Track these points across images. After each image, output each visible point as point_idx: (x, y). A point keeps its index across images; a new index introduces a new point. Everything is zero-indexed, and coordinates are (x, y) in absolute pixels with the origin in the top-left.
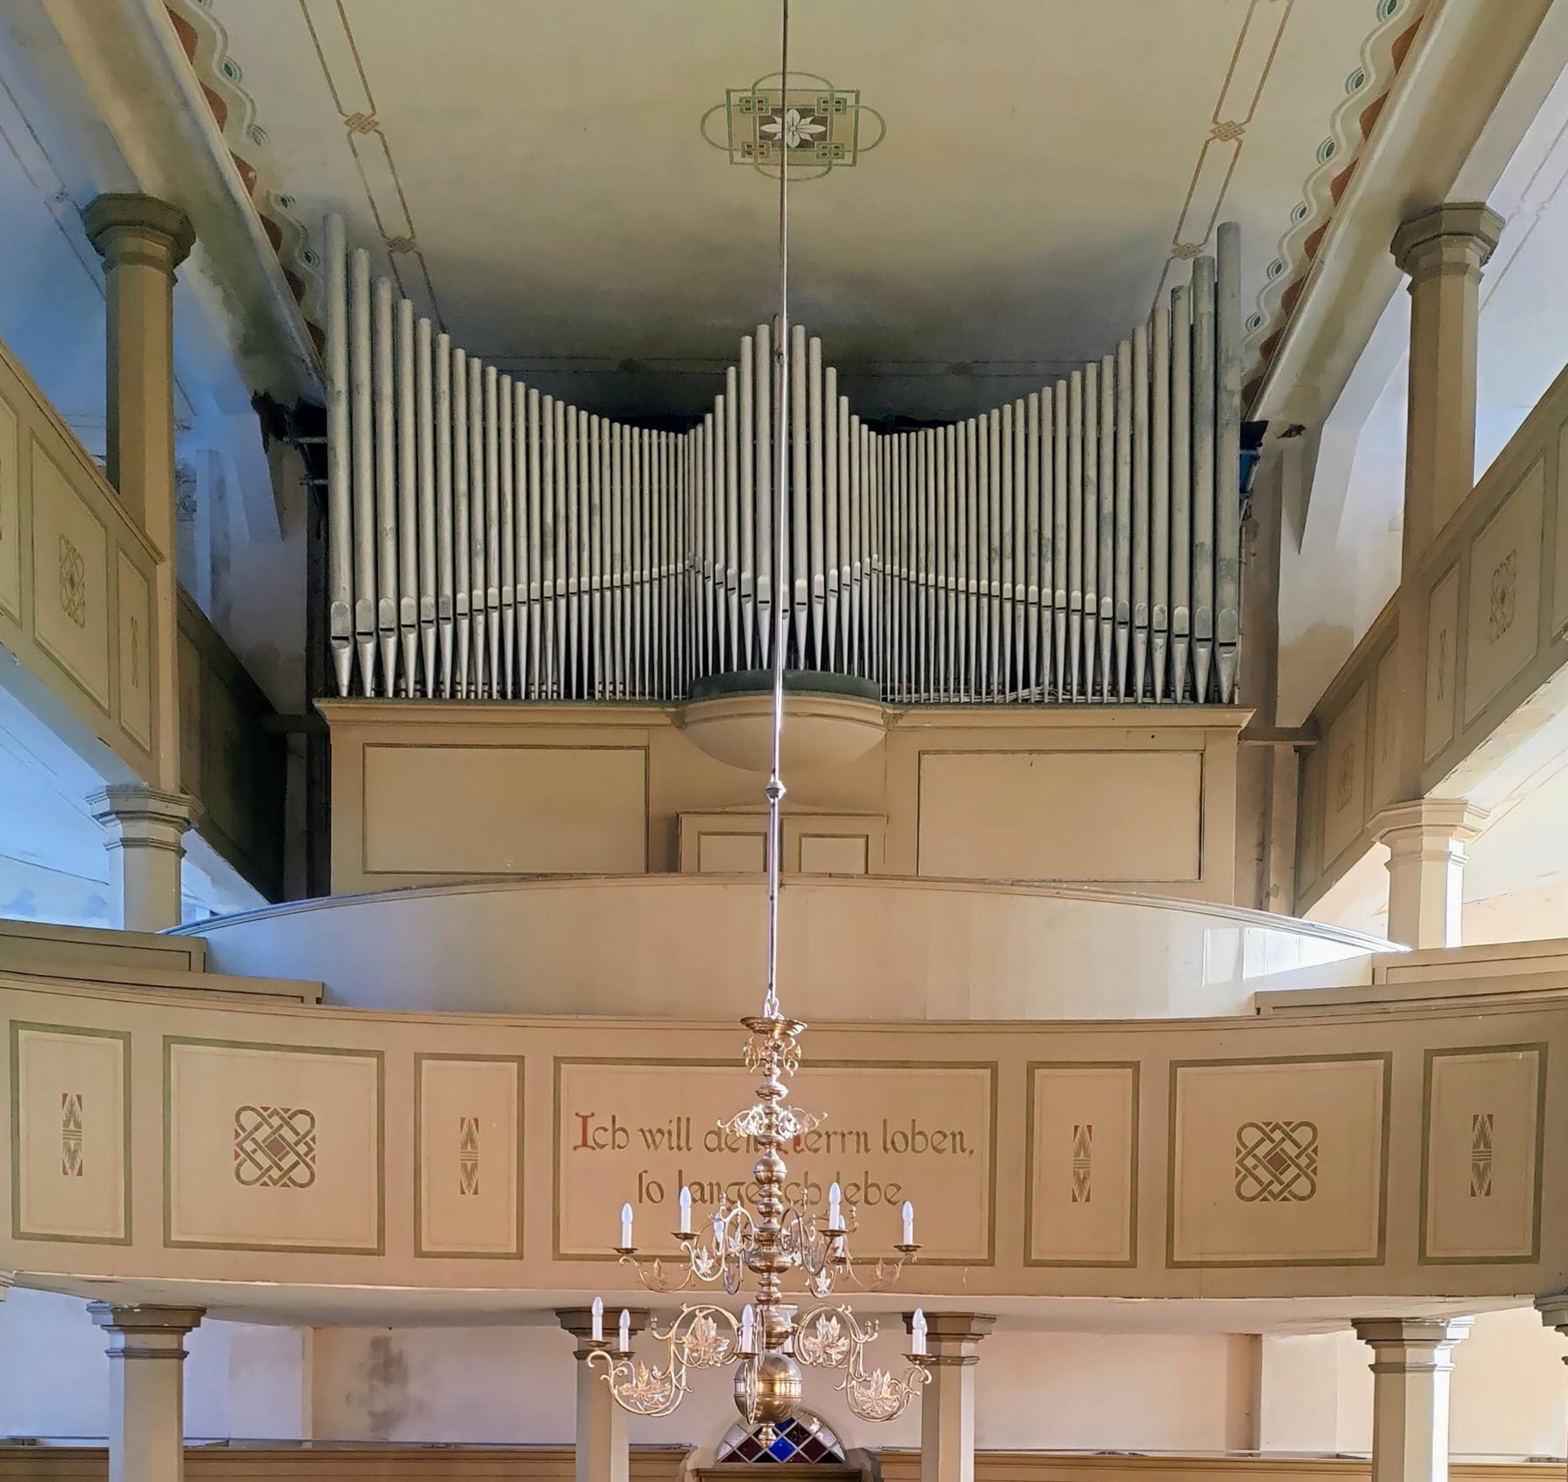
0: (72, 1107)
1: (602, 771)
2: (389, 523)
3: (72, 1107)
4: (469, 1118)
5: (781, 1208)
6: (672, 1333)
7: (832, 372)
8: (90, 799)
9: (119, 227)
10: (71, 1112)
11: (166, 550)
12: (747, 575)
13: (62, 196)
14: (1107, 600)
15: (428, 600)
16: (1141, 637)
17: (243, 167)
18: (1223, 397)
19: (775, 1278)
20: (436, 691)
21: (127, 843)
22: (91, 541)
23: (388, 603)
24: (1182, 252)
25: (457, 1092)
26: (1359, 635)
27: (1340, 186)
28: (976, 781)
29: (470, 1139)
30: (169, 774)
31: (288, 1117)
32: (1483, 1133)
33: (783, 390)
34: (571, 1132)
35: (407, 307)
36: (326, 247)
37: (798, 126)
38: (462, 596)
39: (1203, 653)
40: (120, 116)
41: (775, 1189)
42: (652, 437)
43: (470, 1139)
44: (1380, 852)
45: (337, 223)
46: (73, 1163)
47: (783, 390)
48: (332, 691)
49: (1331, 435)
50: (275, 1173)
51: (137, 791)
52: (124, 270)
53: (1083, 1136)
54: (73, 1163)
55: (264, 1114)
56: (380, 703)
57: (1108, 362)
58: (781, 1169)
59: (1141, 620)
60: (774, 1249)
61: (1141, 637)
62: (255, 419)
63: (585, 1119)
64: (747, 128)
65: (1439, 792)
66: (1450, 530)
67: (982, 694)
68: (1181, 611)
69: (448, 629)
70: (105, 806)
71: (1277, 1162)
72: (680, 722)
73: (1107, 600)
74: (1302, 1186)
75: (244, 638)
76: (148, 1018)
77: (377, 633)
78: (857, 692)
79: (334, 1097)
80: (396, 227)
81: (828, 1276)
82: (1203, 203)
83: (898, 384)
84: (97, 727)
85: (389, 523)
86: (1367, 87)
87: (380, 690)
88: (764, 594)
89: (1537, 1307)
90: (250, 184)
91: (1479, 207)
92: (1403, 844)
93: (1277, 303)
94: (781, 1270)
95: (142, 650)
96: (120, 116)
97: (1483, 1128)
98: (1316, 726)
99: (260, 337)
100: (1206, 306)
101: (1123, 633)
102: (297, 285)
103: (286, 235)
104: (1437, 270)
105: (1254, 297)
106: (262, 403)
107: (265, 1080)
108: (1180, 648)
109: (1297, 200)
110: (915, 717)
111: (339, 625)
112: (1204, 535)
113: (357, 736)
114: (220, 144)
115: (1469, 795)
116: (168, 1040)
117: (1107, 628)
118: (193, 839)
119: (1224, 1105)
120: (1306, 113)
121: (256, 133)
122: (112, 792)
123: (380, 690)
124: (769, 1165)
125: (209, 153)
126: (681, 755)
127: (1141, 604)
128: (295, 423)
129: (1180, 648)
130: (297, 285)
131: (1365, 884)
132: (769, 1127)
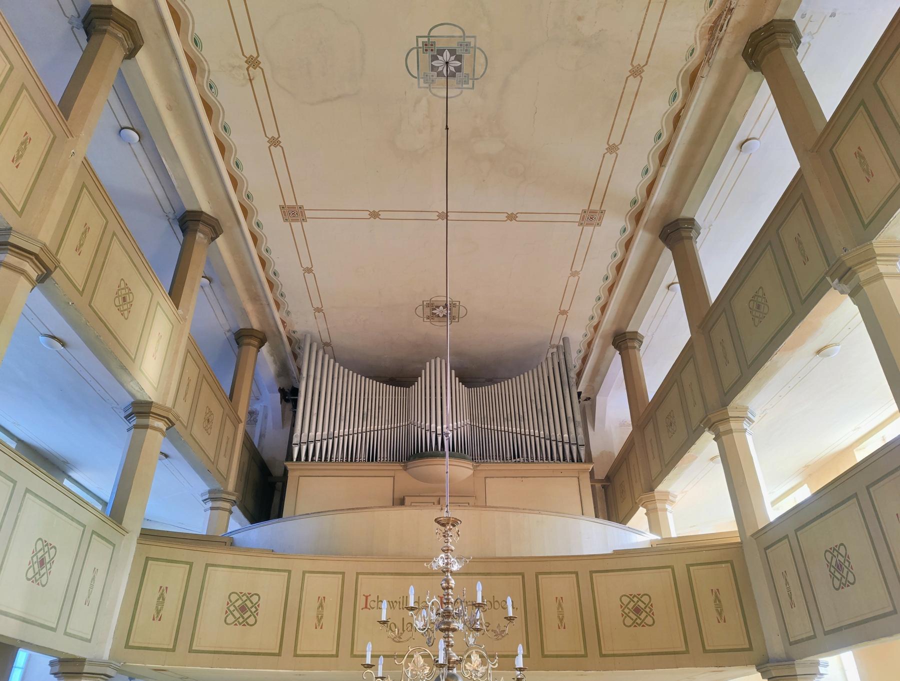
0: (163, 591)
1: (380, 481)
2: (315, 411)
3: (163, 591)
4: (322, 597)
5: (453, 600)
6: (403, 662)
7: (453, 372)
8: (202, 495)
9: (243, 337)
10: (162, 594)
11: (243, 420)
12: (428, 424)
13: (229, 330)
14: (542, 432)
15: (325, 433)
16: (554, 443)
17: (283, 322)
18: (570, 380)
19: (451, 634)
20: (326, 459)
21: (212, 509)
22: (218, 412)
23: (312, 434)
24: (552, 347)
25: (322, 586)
26: (616, 455)
27: (596, 328)
28: (502, 483)
29: (321, 606)
30: (231, 486)
31: (249, 596)
32: (716, 596)
33: (440, 379)
34: (361, 602)
35: (327, 356)
36: (305, 345)
37: (441, 311)
38: (336, 432)
39: (574, 448)
40: (249, 307)
41: (450, 591)
42: (399, 389)
43: (321, 606)
44: (642, 511)
45: (309, 336)
46: (158, 616)
47: (440, 379)
48: (292, 460)
49: (599, 399)
50: (241, 620)
51: (219, 491)
52: (244, 348)
53: (560, 601)
54: (158, 616)
55: (240, 595)
56: (306, 463)
57: (535, 370)
58: (452, 583)
59: (553, 438)
60: (450, 620)
61: (554, 443)
62: (279, 395)
63: (366, 607)
64: (428, 311)
65: (660, 488)
66: (645, 414)
67: (504, 459)
68: (566, 435)
69: (331, 441)
70: (207, 496)
71: (637, 610)
72: (405, 468)
73: (542, 432)
74: (651, 622)
75: (266, 455)
76: (200, 556)
77: (308, 443)
78: (464, 458)
79: (268, 587)
80: (326, 339)
81: (473, 637)
82: (557, 333)
83: (474, 374)
84: (205, 468)
85: (315, 411)
86: (627, 233)
87: (307, 460)
88: (433, 429)
89: (758, 670)
90: (284, 327)
91: (637, 332)
92: (650, 506)
93: (580, 361)
94: (454, 630)
95: (230, 445)
96: (249, 307)
97: (716, 594)
98: (608, 478)
99: (283, 370)
100: (562, 357)
101: (548, 442)
102: (295, 356)
103: (294, 341)
104: (627, 348)
105: (575, 359)
106: (281, 391)
107: (242, 581)
108: (567, 447)
109: (584, 332)
110: (483, 467)
111: (296, 440)
112: (539, 407)
113: (297, 473)
114: (277, 315)
115: (670, 490)
116: (207, 565)
117: (543, 440)
118: (236, 509)
119: (612, 591)
120: (584, 309)
121: (288, 313)
122: (210, 492)
123: (307, 460)
124: (447, 581)
125: (274, 318)
126: (405, 479)
127: (553, 434)
128: (290, 396)
129: (567, 447)
130: (295, 356)
131: (640, 517)
132: (447, 564)
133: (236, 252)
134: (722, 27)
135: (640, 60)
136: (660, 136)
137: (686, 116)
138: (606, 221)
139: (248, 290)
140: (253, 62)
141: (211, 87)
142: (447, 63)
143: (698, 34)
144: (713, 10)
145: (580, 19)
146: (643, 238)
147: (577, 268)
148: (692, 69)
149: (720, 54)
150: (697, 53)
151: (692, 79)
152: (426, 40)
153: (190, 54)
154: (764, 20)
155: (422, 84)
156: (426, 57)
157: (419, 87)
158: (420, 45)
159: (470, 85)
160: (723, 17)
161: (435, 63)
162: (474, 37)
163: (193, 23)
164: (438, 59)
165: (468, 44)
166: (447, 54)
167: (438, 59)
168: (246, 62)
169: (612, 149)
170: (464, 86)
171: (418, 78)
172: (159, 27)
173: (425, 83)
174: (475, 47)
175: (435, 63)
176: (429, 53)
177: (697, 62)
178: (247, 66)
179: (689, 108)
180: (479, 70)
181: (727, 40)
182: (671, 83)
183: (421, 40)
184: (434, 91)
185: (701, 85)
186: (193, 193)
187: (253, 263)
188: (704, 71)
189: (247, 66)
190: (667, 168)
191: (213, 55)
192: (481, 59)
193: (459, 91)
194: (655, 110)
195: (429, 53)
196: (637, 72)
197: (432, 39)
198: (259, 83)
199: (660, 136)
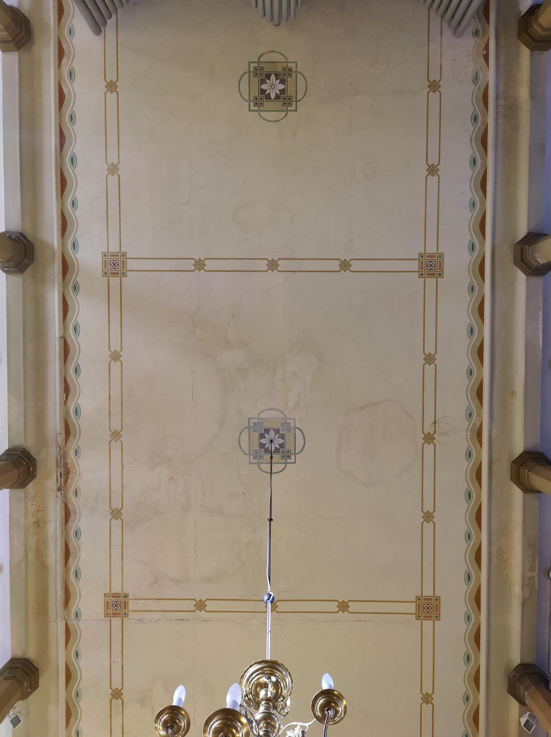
17: (486, 57)
90: (487, 47)
133: (507, 203)
134: (61, 477)
135: (116, 446)
136: (74, 246)
137: (60, 394)
138: (100, 608)
139: (516, 128)
140: (429, 438)
141: (470, 415)
142: (272, 441)
143: (77, 468)
144: (73, 486)
145: (171, 479)
146: (51, 234)
147: (112, 180)
148: (71, 438)
149: (53, 451)
150: (72, 452)
151: (68, 430)
152: (288, 461)
153: (477, 443)
154: (31, 486)
155: (292, 422)
156: (291, 91)
157: (294, 419)
158: (293, 456)
159: (252, 421)
160: (63, 483)
161: (281, 441)
162: (251, 463)
163: (472, 100)
164: (279, 445)
165: (255, 457)
166: (272, 433)
167: (279, 445)
168: (434, 439)
169: (116, 356)
170: (256, 421)
171: (296, 428)
172: (494, 467)
173: (290, 423)
174: (250, 455)
175: (281, 441)
176: (286, 450)
177: (69, 444)
178: (435, 436)
179: (60, 404)
180: (245, 436)
181: (52, 464)
182: (83, 423)
183: (292, 460)
184: (281, 416)
185: (58, 427)
186: (528, 301)
187: (495, 183)
188: (61, 439)
189: (435, 436)
190: (57, 335)
191: (462, 441)
192: (245, 445)
193: (262, 416)
194: (90, 398)
195: (286, 450)
196: (116, 435)
197: (284, 461)
198: (429, 420)
199: (74, 246)
